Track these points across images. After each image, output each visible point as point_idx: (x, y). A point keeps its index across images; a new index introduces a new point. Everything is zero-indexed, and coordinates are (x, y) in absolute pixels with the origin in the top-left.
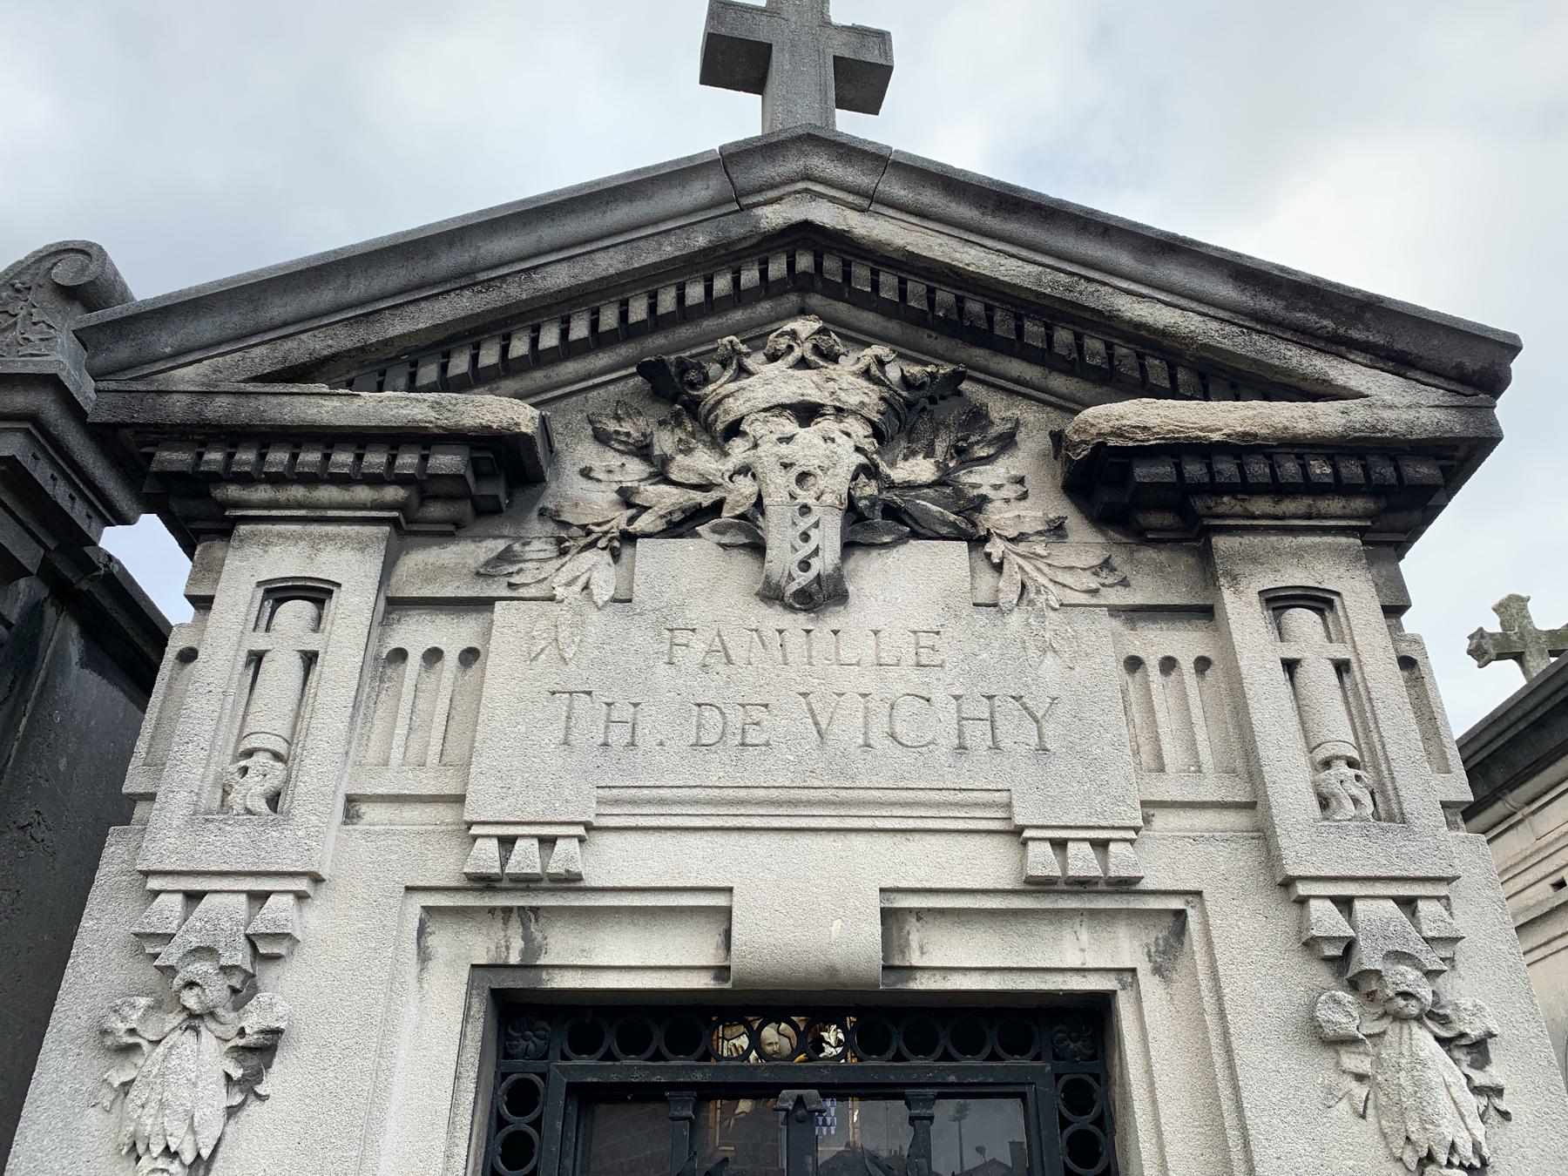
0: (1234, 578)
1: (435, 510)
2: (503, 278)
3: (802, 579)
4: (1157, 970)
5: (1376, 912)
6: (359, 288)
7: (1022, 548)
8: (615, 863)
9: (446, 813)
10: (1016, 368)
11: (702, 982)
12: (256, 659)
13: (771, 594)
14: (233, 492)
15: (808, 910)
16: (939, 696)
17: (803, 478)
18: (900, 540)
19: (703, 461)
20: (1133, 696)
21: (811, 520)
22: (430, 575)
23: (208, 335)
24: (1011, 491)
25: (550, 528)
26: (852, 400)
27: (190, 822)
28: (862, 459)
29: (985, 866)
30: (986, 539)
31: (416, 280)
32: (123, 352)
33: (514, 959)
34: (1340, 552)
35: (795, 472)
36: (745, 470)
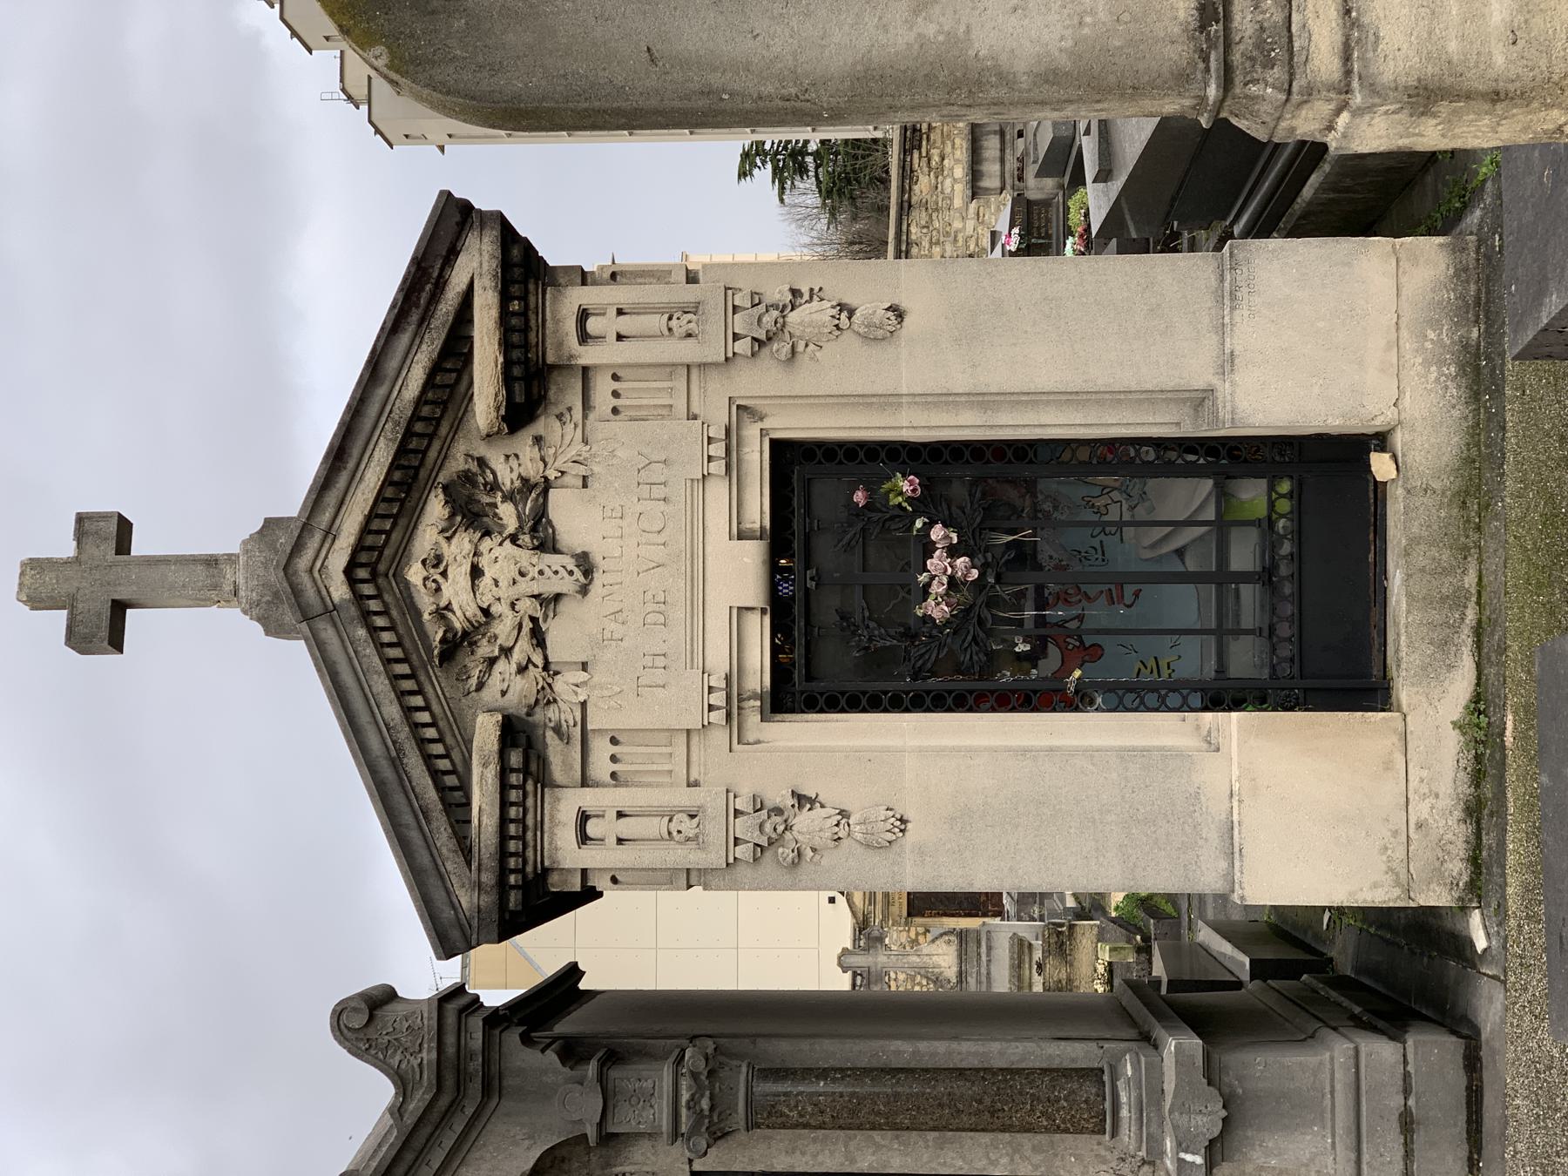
0: (571, 357)
1: (533, 767)
2: (394, 743)
3: (578, 574)
4: (761, 419)
5: (740, 323)
6: (408, 818)
7: (550, 461)
8: (719, 659)
9: (695, 739)
10: (432, 454)
11: (767, 619)
12: (620, 841)
13: (584, 590)
14: (529, 869)
15: (739, 573)
16: (639, 508)
17: (522, 574)
18: (549, 522)
19: (503, 629)
20: (633, 413)
21: (547, 570)
22: (567, 766)
23: (1100, 382)
24: (513, 462)
25: (538, 709)
26: (467, 547)
27: (703, 849)
28: (507, 542)
29: (719, 493)
30: (546, 478)
31: (399, 789)
32: (455, 934)
33: (758, 703)
34: (555, 299)
35: (518, 578)
36: (513, 605)
